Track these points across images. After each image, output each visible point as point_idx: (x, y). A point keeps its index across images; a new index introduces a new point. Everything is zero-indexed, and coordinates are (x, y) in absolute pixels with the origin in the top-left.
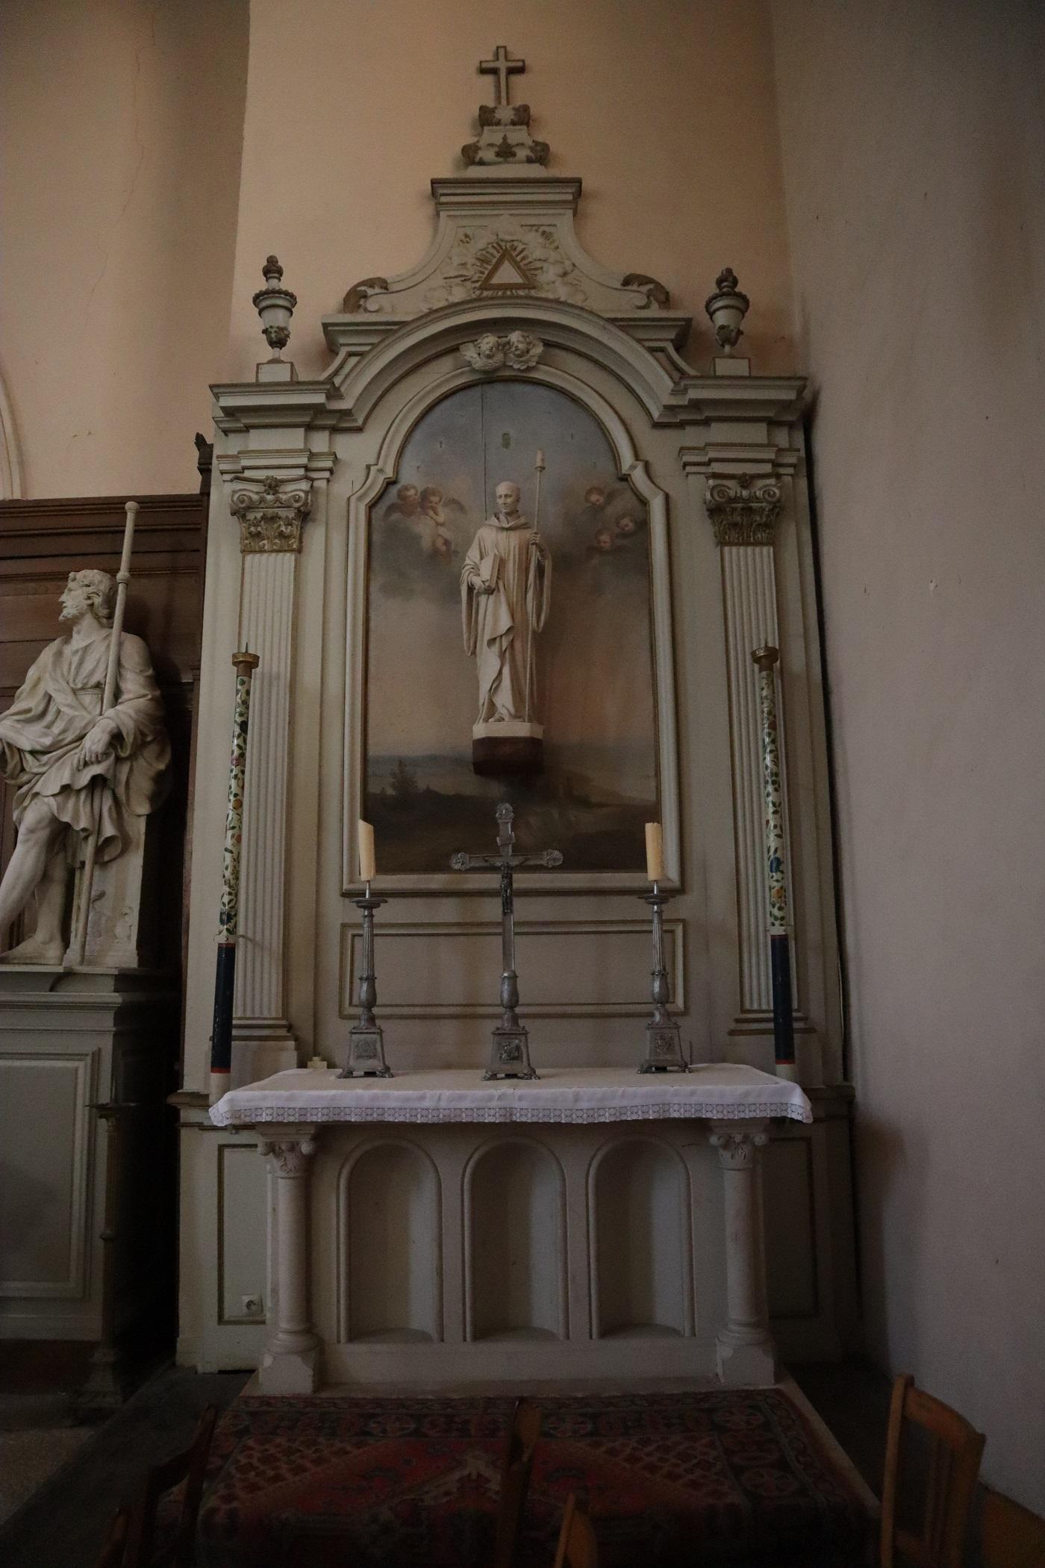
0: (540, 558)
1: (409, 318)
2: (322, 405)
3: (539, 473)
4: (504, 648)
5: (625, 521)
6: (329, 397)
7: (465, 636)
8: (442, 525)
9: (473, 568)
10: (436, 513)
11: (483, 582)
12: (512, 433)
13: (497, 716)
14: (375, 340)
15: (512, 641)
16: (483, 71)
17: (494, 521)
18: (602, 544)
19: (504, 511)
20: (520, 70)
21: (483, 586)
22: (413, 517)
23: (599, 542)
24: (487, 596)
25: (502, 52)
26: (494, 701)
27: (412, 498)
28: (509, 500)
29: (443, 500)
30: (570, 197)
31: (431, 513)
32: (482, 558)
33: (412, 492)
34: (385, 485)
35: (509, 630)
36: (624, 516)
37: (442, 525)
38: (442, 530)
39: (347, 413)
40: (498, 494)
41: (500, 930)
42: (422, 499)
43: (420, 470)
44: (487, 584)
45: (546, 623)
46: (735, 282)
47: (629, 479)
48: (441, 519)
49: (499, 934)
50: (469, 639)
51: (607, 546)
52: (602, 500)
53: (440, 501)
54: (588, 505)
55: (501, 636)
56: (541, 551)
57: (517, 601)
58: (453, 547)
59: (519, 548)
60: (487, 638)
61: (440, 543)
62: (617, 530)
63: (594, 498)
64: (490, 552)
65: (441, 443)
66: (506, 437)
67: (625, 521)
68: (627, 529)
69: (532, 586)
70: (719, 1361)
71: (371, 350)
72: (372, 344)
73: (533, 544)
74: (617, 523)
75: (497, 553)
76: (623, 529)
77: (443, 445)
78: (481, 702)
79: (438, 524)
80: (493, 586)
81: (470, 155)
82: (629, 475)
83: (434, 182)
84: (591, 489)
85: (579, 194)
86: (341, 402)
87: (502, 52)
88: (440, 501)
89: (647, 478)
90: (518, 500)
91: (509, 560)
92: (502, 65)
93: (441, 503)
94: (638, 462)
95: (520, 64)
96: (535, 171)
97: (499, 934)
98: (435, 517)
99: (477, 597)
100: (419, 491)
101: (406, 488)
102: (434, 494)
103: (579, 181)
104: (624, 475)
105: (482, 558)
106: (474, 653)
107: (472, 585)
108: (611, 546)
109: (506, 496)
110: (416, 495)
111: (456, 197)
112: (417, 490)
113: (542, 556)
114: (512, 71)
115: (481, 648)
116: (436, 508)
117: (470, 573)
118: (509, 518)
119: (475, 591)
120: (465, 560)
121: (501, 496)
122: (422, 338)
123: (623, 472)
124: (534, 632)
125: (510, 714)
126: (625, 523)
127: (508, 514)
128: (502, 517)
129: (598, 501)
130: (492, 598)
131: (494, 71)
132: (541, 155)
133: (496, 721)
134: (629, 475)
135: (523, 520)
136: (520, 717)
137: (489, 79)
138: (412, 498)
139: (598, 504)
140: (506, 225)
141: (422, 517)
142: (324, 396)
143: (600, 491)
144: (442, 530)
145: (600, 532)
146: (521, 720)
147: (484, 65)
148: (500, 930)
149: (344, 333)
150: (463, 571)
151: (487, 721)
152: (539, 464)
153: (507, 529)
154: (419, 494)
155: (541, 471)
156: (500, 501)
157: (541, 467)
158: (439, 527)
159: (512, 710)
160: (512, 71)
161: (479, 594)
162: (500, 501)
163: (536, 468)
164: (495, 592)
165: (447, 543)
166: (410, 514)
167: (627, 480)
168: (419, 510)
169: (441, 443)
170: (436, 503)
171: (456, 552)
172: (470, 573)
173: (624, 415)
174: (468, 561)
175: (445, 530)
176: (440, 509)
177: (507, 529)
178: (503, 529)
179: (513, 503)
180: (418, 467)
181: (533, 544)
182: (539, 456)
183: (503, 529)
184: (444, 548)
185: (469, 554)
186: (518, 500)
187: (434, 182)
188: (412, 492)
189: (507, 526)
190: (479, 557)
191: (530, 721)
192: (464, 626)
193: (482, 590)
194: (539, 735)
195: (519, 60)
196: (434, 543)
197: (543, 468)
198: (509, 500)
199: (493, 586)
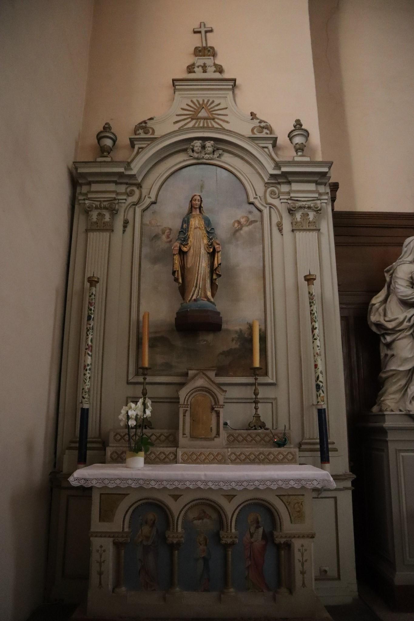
1: (159, 136)
2: (123, 172)
6: (126, 169)
14: (149, 143)
16: (195, 32)
20: (211, 31)
25: (202, 25)
30: (231, 87)
34: (151, 203)
39: (133, 176)
41: (185, 403)
46: (301, 125)
49: (184, 402)
70: (258, 377)
71: (147, 146)
72: (148, 144)
81: (191, 69)
83: (174, 80)
85: (235, 85)
86: (132, 171)
87: (202, 25)
92: (203, 30)
95: (210, 29)
96: (217, 75)
97: (184, 402)
103: (235, 80)
111: (199, 86)
114: (206, 32)
122: (156, 151)
131: (200, 32)
132: (220, 69)
137: (198, 35)
140: (200, 96)
142: (123, 169)
147: (195, 30)
148: (185, 403)
149: (136, 141)
160: (206, 32)
187: (174, 80)
195: (209, 28)
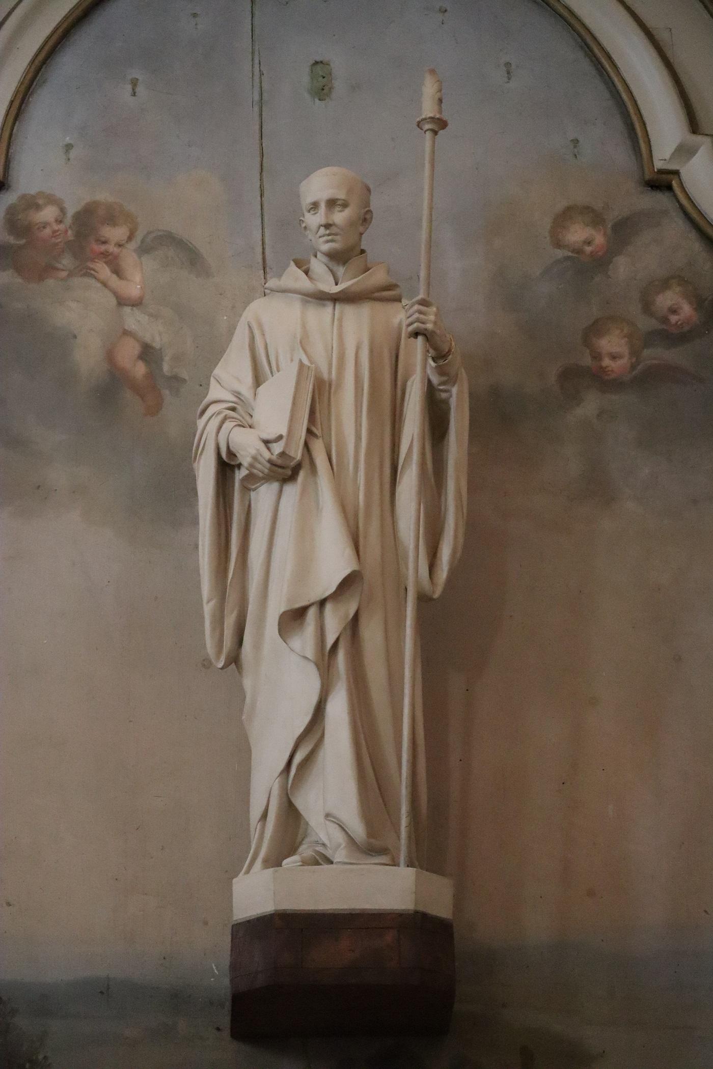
0: (435, 380)
3: (429, 135)
4: (330, 641)
5: (667, 299)
7: (208, 609)
8: (137, 304)
9: (233, 409)
10: (117, 271)
11: (266, 442)
12: (340, 65)
13: (306, 850)
15: (356, 618)
17: (294, 277)
18: (606, 362)
19: (326, 247)
21: (267, 455)
22: (50, 282)
23: (597, 357)
24: (275, 486)
26: (294, 802)
27: (48, 231)
28: (340, 217)
29: (139, 236)
31: (104, 271)
32: (258, 381)
33: (48, 214)
35: (348, 584)
36: (665, 284)
37: (137, 304)
38: (133, 320)
40: (307, 200)
42: (78, 235)
43: (73, 154)
44: (277, 448)
45: (453, 572)
47: (675, 184)
48: (133, 289)
50: (219, 620)
51: (616, 367)
52: (599, 239)
53: (130, 238)
54: (560, 253)
55: (322, 603)
56: (440, 356)
57: (368, 506)
58: (166, 368)
59: (371, 351)
60: (277, 605)
61: (128, 354)
62: (646, 324)
63: (577, 234)
64: (283, 364)
65: (134, 83)
66: (319, 69)
67: (667, 299)
68: (674, 319)
69: (415, 457)
73: (416, 334)
74: (647, 307)
75: (306, 361)
76: (665, 320)
77: (140, 89)
78: (255, 812)
79: (122, 302)
80: (297, 453)
82: (676, 173)
84: (569, 209)
88: (130, 238)
89: (428, 576)
90: (365, 219)
91: (339, 385)
93: (133, 245)
94: (698, 139)
98: (114, 280)
99: (246, 489)
100: (71, 211)
101: (32, 203)
102: (112, 217)
104: (661, 172)
105: (258, 381)
106: (235, 660)
107: (231, 454)
108: (633, 367)
109: (332, 203)
110: (59, 221)
112: (63, 210)
113: (441, 371)
115: (258, 646)
116: (116, 257)
117: (225, 418)
118: (341, 270)
119: (240, 474)
120: (207, 389)
121: (315, 206)
123: (658, 165)
124: (423, 599)
125: (351, 840)
126: (669, 303)
127: (338, 257)
128: (318, 266)
129: (589, 243)
130: (292, 491)
133: (305, 863)
134: (676, 173)
135: (378, 277)
136: (383, 851)
138: (48, 231)
139: (588, 249)
141: (77, 281)
143: (595, 217)
144: (133, 320)
145: (595, 329)
146: (384, 859)
150: (201, 423)
151: (279, 865)
152: (428, 109)
153: (335, 299)
154: (68, 220)
155: (435, 133)
156: (314, 220)
157: (432, 119)
158: (127, 310)
159: (358, 829)
161: (251, 479)
162: (314, 220)
163: (419, 125)
164: (302, 475)
165: (148, 353)
166: (44, 271)
167: (669, 188)
168: (67, 261)
169: (134, 83)
170: (120, 245)
171: (175, 381)
172: (225, 418)
173: (651, 23)
174: (215, 392)
175: (144, 319)
176: (129, 259)
177: (335, 299)
178: (322, 298)
179: (351, 224)
180: (69, 147)
181: (416, 334)
182: (429, 89)
183: (322, 298)
184: (140, 370)
185: (217, 371)
186: (365, 219)
188: (48, 214)
189: (335, 289)
190: (249, 378)
191: (410, 864)
192: (423, 246)
193: (263, 468)
194: (442, 909)
196: (110, 356)
197: (442, 124)
198: (340, 217)
199: (297, 453)
